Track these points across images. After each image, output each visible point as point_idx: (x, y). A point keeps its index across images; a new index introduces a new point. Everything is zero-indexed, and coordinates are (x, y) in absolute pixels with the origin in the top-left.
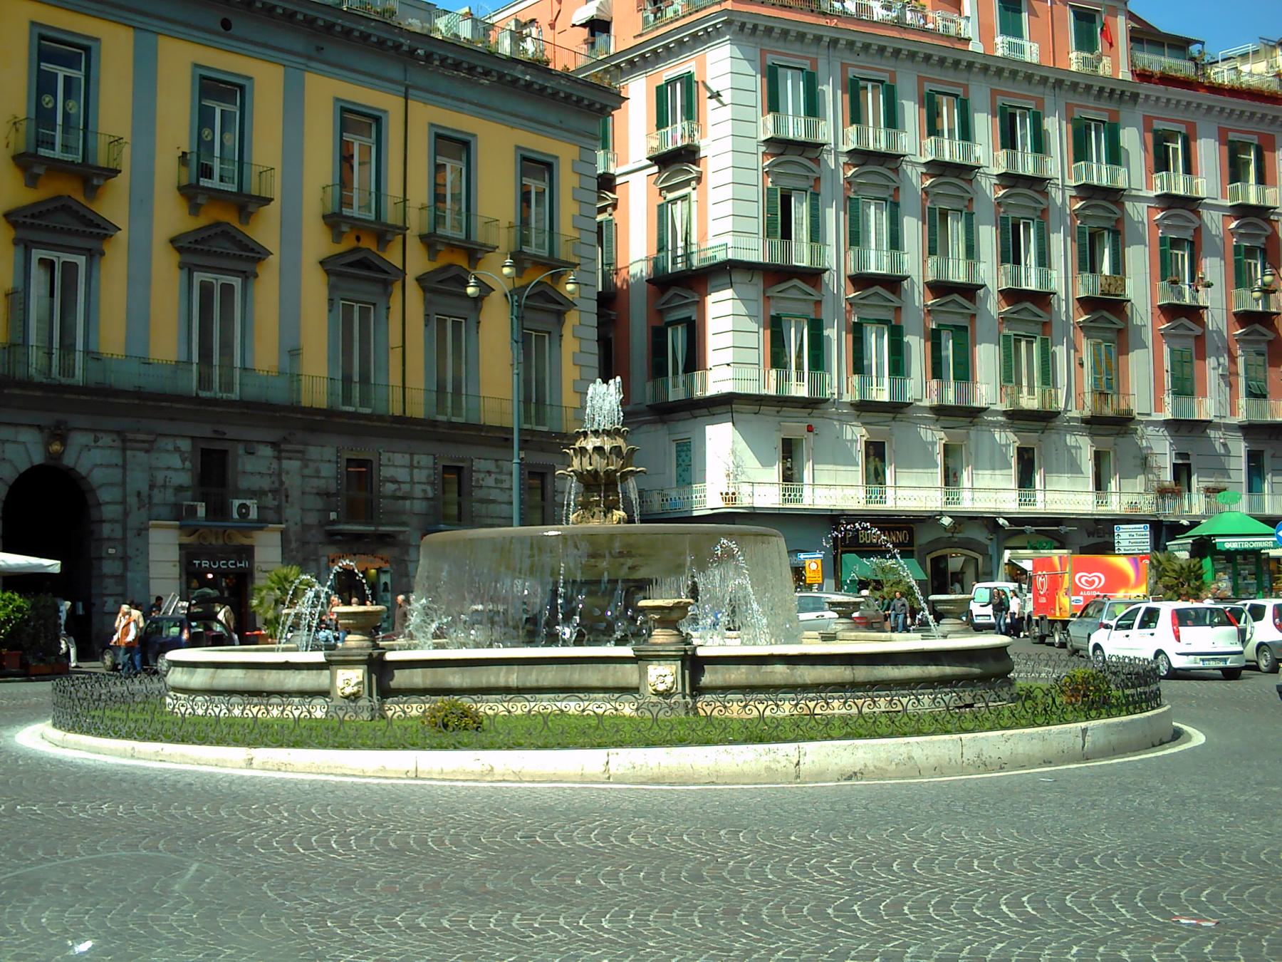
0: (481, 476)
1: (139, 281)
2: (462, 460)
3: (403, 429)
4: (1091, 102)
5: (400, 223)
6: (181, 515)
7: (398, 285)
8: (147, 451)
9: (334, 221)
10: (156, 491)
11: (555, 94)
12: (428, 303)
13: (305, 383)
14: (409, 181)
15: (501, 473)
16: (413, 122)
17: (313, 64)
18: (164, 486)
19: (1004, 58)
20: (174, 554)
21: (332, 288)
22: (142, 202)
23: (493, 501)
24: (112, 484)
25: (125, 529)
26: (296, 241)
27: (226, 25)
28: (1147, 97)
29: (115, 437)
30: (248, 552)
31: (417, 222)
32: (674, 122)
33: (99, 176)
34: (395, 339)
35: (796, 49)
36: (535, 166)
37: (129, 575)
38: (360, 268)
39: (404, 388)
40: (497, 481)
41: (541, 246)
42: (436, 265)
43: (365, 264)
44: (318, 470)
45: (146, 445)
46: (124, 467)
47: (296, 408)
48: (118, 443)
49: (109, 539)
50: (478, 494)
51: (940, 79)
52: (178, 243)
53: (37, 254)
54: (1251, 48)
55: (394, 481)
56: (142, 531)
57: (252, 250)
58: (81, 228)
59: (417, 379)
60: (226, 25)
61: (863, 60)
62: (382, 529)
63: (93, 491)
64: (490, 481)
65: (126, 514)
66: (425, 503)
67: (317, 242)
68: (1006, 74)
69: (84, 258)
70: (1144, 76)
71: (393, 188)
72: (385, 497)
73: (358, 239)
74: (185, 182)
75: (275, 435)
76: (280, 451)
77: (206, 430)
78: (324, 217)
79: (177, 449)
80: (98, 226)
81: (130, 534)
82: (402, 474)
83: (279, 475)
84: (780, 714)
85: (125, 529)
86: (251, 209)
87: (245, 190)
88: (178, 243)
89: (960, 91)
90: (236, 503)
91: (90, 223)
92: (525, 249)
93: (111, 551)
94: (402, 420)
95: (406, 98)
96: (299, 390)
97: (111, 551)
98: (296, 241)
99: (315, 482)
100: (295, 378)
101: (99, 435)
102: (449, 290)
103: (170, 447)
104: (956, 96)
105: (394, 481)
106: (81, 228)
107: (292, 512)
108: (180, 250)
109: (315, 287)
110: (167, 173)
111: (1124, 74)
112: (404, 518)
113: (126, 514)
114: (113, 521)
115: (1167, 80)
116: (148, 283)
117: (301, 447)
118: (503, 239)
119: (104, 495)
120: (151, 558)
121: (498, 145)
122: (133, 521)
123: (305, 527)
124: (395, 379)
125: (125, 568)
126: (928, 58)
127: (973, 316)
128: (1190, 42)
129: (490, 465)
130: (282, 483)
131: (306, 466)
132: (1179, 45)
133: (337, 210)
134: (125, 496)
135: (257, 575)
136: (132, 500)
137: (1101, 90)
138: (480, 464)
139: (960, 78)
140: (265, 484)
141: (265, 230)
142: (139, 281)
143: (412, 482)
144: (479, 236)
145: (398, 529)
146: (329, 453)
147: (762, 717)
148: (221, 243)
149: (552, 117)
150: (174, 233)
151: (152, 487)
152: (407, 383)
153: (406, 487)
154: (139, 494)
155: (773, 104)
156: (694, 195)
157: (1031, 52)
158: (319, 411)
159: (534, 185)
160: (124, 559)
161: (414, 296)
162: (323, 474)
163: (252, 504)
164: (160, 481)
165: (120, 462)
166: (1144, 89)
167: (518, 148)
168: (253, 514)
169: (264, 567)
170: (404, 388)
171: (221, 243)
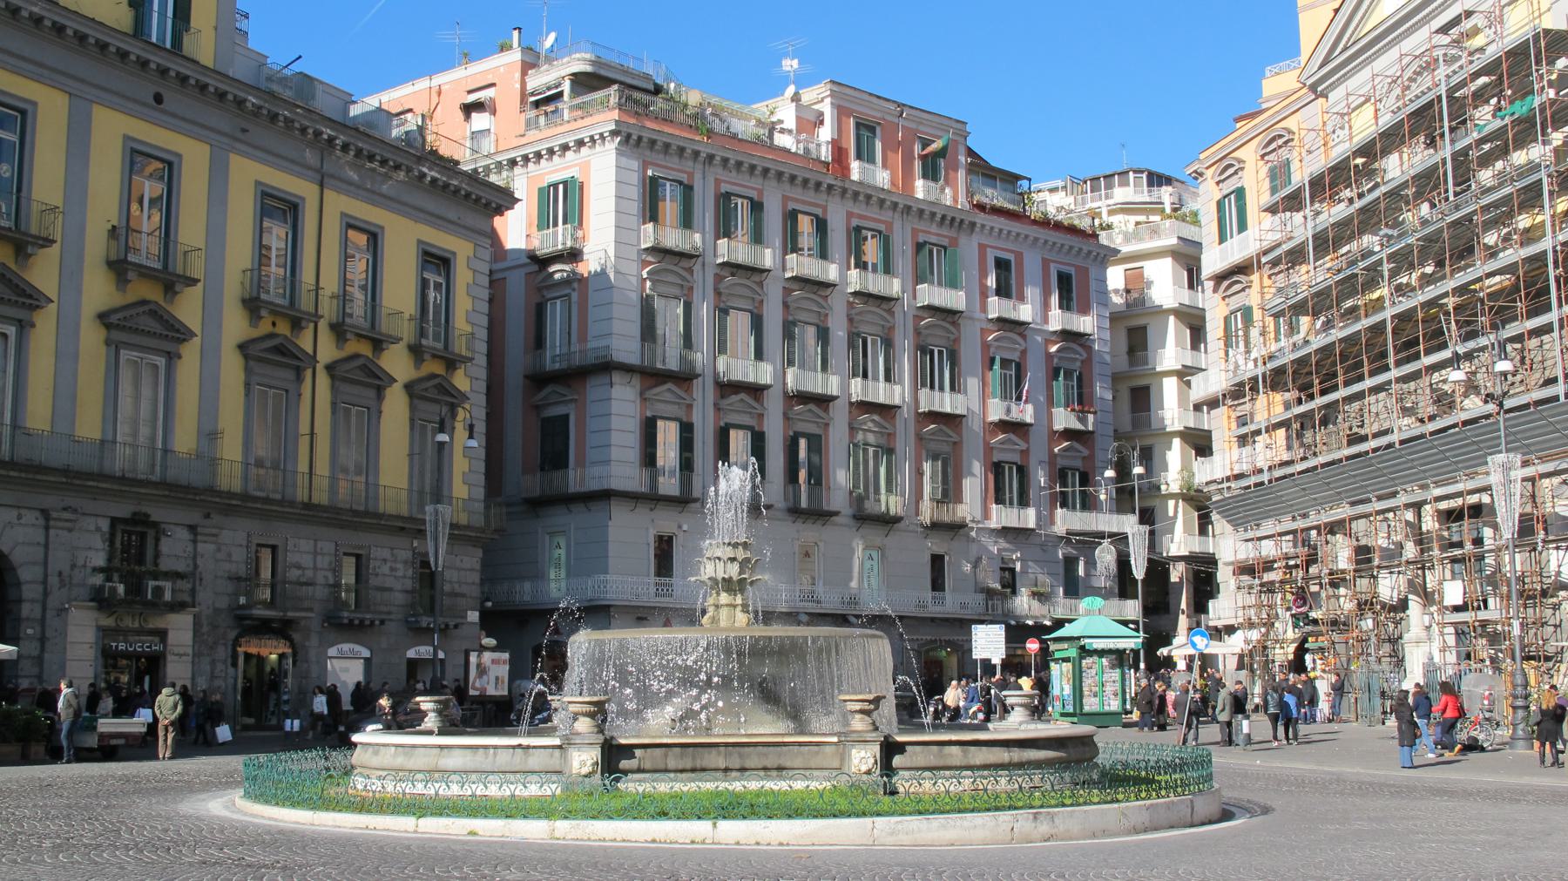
0: (378, 563)
1: (66, 356)
2: (361, 547)
3: (313, 514)
4: (934, 228)
5: (312, 310)
6: (101, 601)
7: (309, 373)
8: (70, 530)
9: (253, 305)
10: (76, 571)
11: (457, 191)
12: (333, 388)
13: (224, 469)
14: (326, 270)
15: (395, 561)
16: (330, 210)
17: (238, 145)
18: (84, 566)
19: (860, 183)
20: (90, 635)
21: (248, 371)
22: (71, 274)
23: (390, 590)
24: (34, 564)
25: (44, 609)
26: (217, 321)
27: (158, 99)
28: (983, 226)
29: (38, 514)
30: (162, 634)
31: (328, 310)
32: (556, 224)
33: (34, 244)
34: (304, 428)
35: (674, 161)
36: (436, 261)
37: (47, 656)
38: (274, 357)
39: (311, 473)
40: (392, 569)
41: (436, 337)
42: (256, 333)
43: (281, 350)
44: (230, 555)
45: (68, 525)
46: (46, 546)
47: (212, 490)
48: (42, 522)
49: (28, 619)
50: (373, 581)
51: (733, 182)
52: (103, 317)
53: (125, 354)
54: (1060, 184)
55: (299, 567)
56: (62, 612)
57: (178, 331)
58: (14, 298)
59: (323, 468)
60: (158, 99)
61: (733, 176)
62: (290, 614)
63: (13, 569)
64: (386, 569)
65: (46, 594)
66: (326, 590)
67: (236, 326)
68: (861, 198)
69: (13, 329)
70: (981, 207)
71: (307, 276)
72: (290, 583)
73: (274, 324)
74: (113, 257)
75: (194, 517)
76: (196, 535)
77: (124, 510)
78: (244, 301)
79: (98, 529)
80: (30, 297)
81: (49, 614)
82: (306, 561)
83: (195, 558)
84: (526, 793)
85: (44, 609)
86: (177, 288)
87: (171, 269)
88: (103, 317)
89: (882, 227)
90: (152, 584)
91: (23, 293)
92: (424, 342)
93: (30, 631)
94: (308, 506)
95: (322, 186)
96: (377, 498)
97: (30, 631)
98: (217, 321)
99: (227, 566)
100: (214, 462)
101: (23, 512)
102: (361, 380)
103: (92, 528)
104: (680, 183)
105: (299, 567)
106: (14, 298)
107: (205, 597)
108: (108, 326)
109: (232, 369)
110: (96, 246)
111: (962, 202)
112: (306, 604)
113: (46, 594)
114: (33, 601)
115: (998, 211)
116: (76, 357)
117: (214, 531)
118: (407, 332)
119: (25, 574)
120: (69, 639)
121: (404, 238)
122: (53, 602)
123: (217, 611)
124: (303, 466)
125: (43, 649)
126: (793, 178)
127: (827, 425)
128: (1017, 177)
129: (386, 553)
130: (196, 566)
131: (219, 550)
132: (1011, 179)
133: (255, 294)
134: (46, 576)
135: (170, 658)
136: (53, 580)
137: (944, 217)
138: (377, 553)
139: (821, 198)
140: (181, 567)
141: (188, 309)
142: (66, 356)
143: (315, 568)
144: (385, 326)
145: (297, 614)
146: (241, 537)
147: (473, 795)
148: (145, 324)
149: (452, 214)
150: (103, 308)
151: (73, 566)
152: (317, 468)
153: (309, 573)
154: (60, 574)
155: (652, 213)
156: (575, 296)
157: (882, 178)
158: (231, 495)
159: (432, 278)
160: (43, 640)
161: (323, 381)
162: (234, 558)
163: (167, 585)
164: (80, 562)
165: (42, 540)
166: (981, 218)
167: (420, 242)
168: (168, 596)
169: (176, 650)
170: (311, 473)
171: (145, 324)
